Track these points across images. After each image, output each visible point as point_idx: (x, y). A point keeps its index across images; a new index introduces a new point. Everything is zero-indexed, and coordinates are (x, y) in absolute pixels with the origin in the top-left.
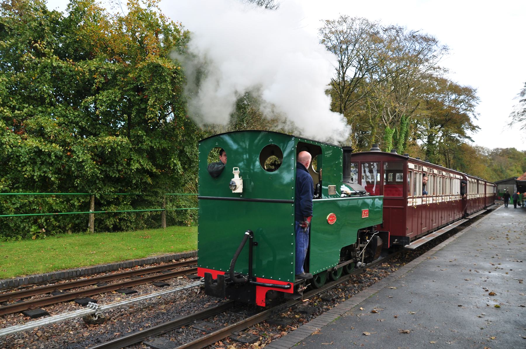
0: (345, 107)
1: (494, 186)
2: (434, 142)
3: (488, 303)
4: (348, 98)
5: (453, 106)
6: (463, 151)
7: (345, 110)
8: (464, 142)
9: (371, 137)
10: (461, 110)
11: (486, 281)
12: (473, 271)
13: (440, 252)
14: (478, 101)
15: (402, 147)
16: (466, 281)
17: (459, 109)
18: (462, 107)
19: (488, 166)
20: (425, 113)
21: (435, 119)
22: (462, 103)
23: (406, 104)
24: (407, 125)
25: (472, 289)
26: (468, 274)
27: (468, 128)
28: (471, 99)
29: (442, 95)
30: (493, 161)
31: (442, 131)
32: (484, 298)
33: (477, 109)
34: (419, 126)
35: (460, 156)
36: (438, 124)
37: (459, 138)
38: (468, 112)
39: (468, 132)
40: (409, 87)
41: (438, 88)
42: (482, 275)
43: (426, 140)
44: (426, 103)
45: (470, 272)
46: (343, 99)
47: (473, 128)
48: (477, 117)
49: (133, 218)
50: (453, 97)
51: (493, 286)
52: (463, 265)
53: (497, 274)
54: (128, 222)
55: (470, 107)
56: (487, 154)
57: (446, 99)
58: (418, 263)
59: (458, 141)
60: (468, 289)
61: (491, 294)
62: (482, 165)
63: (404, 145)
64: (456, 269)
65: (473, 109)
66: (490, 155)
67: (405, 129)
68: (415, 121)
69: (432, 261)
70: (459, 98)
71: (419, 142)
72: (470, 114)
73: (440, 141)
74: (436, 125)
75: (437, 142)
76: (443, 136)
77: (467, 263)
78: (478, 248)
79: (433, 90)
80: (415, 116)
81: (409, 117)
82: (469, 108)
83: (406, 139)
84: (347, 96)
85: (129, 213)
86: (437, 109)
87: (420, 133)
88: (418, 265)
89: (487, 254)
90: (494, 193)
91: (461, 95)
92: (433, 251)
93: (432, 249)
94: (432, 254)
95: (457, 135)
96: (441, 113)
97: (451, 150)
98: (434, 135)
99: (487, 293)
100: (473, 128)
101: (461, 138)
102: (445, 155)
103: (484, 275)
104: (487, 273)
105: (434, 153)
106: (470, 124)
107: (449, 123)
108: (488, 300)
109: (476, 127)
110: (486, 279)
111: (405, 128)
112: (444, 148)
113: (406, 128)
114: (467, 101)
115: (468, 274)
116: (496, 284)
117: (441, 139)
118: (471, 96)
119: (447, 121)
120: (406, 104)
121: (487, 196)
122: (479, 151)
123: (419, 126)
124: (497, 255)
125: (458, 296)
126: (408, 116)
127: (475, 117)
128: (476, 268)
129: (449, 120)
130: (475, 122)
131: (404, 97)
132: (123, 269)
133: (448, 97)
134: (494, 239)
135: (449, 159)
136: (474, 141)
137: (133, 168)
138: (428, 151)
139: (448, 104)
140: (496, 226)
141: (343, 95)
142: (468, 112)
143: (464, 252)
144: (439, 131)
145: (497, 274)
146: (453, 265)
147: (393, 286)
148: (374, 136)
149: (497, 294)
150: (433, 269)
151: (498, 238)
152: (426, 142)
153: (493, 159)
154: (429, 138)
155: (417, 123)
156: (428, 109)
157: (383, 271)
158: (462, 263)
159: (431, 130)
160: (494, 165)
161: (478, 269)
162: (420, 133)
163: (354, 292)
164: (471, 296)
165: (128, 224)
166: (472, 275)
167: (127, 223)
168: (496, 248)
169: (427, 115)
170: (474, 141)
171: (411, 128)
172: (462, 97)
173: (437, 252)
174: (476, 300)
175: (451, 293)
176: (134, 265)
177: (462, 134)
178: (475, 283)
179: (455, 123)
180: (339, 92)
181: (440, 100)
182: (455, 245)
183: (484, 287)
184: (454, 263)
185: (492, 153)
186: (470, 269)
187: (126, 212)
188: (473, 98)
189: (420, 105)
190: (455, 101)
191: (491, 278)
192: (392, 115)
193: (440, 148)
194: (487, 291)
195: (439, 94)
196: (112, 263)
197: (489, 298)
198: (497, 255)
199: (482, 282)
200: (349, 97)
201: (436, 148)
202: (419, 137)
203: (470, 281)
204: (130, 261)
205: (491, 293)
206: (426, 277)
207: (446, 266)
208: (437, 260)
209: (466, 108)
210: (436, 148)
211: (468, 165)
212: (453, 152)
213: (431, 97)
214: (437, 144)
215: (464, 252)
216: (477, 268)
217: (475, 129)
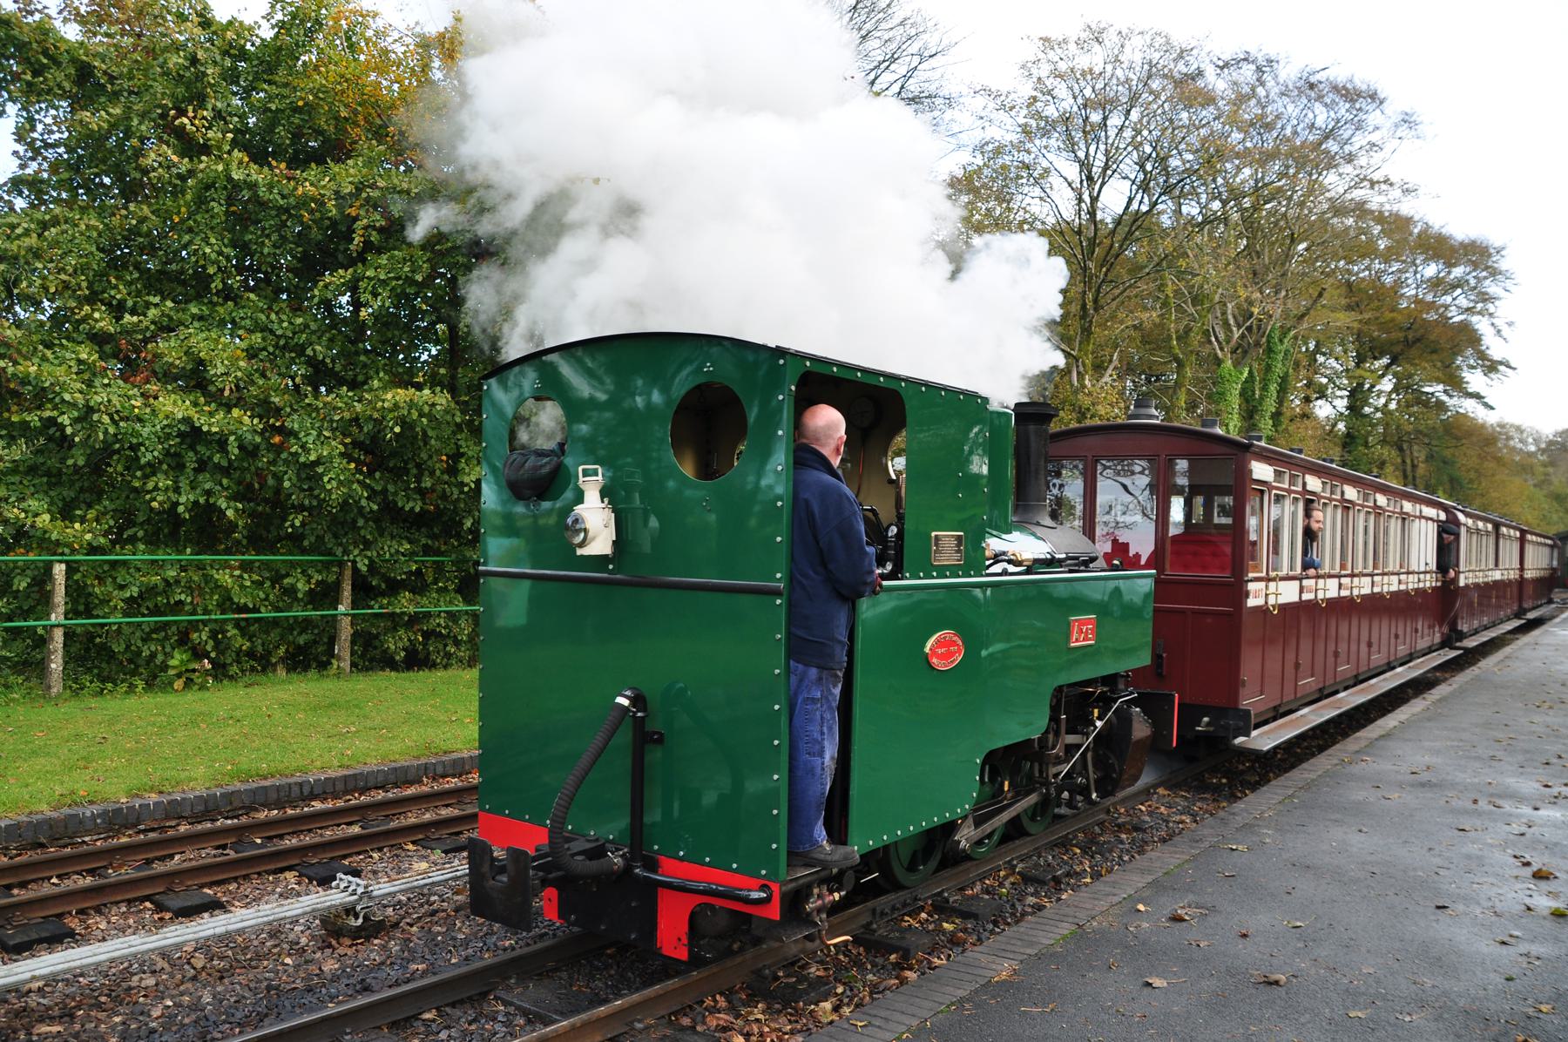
0: (1096, 301)
1: (1552, 547)
2: (1367, 410)
3: (1528, 901)
4: (1106, 275)
5: (1429, 298)
6: (1458, 439)
7: (1096, 310)
8: (1461, 411)
9: (1175, 392)
10: (1453, 312)
11: (1522, 835)
12: (1483, 804)
13: (1382, 743)
14: (1508, 284)
15: (1271, 422)
16: (1461, 833)
17: (1447, 307)
18: (1457, 302)
19: (1535, 486)
20: (1344, 319)
21: (1372, 340)
22: (1459, 291)
23: (1283, 293)
24: (1285, 358)
25: (1479, 858)
26: (1466, 812)
27: (1473, 367)
28: (1486, 278)
30: (1550, 470)
31: (1395, 375)
32: (1519, 886)
33: (1503, 309)
34: (1321, 359)
35: (1447, 453)
37: (1444, 398)
38: (1475, 319)
39: (1475, 380)
40: (1293, 240)
41: (1382, 244)
42: (1511, 815)
43: (1345, 402)
44: (1344, 290)
45: (1474, 806)
47: (1491, 367)
48: (1506, 331)
49: (464, 629)
50: (1431, 270)
51: (1547, 852)
52: (1453, 785)
53: (1558, 815)
54: (450, 642)
55: (1484, 301)
56: (1533, 448)
57: (1407, 279)
58: (1313, 776)
59: (1441, 406)
60: (1469, 857)
61: (1539, 876)
62: (1517, 481)
63: (1276, 416)
64: (1429, 795)
65: (1491, 308)
66: (1544, 451)
67: (1279, 369)
69: (1356, 769)
70: (1449, 273)
71: (1323, 410)
72: (1481, 324)
73: (1386, 405)
74: (1375, 358)
75: (1377, 409)
76: (1396, 390)
77: (1465, 777)
78: (1500, 736)
79: (1369, 251)
81: (1292, 333)
82: (1480, 306)
83: (1281, 401)
84: (1102, 266)
85: (452, 616)
86: (1377, 309)
87: (1324, 381)
88: (1313, 780)
89: (1527, 752)
90: (1553, 569)
91: (1455, 265)
92: (1360, 738)
93: (1358, 734)
94: (1356, 748)
95: (1441, 387)
96: (1393, 320)
98: (1367, 386)
99: (1528, 871)
100: (1491, 367)
101: (1451, 396)
102: (1401, 449)
103: (1519, 816)
104: (1526, 810)
105: (1367, 442)
106: (1482, 356)
107: (1414, 352)
108: (1529, 892)
109: (1501, 363)
110: (1524, 829)
111: (1279, 365)
112: (1398, 427)
113: (1284, 365)
114: (1473, 282)
115: (1466, 812)
116: (1556, 844)
117: (1389, 400)
118: (1487, 268)
119: (1409, 344)
120: (1283, 293)
121: (1528, 575)
122: (1509, 438)
123: (1321, 359)
124: (1560, 757)
125: (1436, 878)
126: (1289, 330)
127: (1499, 331)
128: (1492, 795)
130: (1495, 348)
132: (434, 779)
133: (1416, 272)
134: (1551, 708)
136: (1492, 408)
137: (466, 479)
138: (1348, 435)
139: (1414, 292)
140: (1558, 667)
141: (1091, 265)
142: (1475, 319)
143: (1456, 743)
144: (1383, 376)
145: (1558, 815)
146: (1423, 785)
148: (1183, 389)
149: (1558, 874)
150: (1359, 794)
151: (1562, 706)
153: (1552, 464)
154: (1353, 394)
155: (1317, 350)
156: (1349, 308)
158: (1450, 777)
159: (1359, 372)
160: (1555, 481)
161: (1500, 796)
162: (1324, 381)
164: (1476, 880)
165: (448, 648)
166: (1479, 814)
167: (446, 645)
168: (1557, 736)
170: (1492, 408)
171: (1297, 365)
172: (1458, 272)
173: (1372, 743)
174: (1493, 892)
175: (1415, 869)
176: (467, 767)
177: (1456, 384)
178: (1490, 841)
179: (1434, 352)
180: (1080, 257)
182: (1428, 724)
183: (1518, 854)
184: (1425, 776)
185: (1550, 443)
186: (1474, 796)
187: (445, 612)
188: (1494, 273)
189: (1326, 294)
190: (1436, 284)
191: (1541, 826)
192: (1239, 327)
193: (1387, 426)
194: (1528, 864)
195: (1387, 261)
196: (403, 762)
197: (1531, 886)
198: (1560, 757)
199: (1511, 837)
200: (1108, 270)
201: (1373, 426)
203: (1472, 834)
204: (455, 756)
205: (1540, 870)
206: (1337, 816)
207: (1401, 786)
208: (1372, 765)
209: (1471, 305)
210: (1373, 426)
211: (1471, 481)
212: (1427, 441)
215: (1456, 743)
216: (1498, 796)
217: (1497, 371)
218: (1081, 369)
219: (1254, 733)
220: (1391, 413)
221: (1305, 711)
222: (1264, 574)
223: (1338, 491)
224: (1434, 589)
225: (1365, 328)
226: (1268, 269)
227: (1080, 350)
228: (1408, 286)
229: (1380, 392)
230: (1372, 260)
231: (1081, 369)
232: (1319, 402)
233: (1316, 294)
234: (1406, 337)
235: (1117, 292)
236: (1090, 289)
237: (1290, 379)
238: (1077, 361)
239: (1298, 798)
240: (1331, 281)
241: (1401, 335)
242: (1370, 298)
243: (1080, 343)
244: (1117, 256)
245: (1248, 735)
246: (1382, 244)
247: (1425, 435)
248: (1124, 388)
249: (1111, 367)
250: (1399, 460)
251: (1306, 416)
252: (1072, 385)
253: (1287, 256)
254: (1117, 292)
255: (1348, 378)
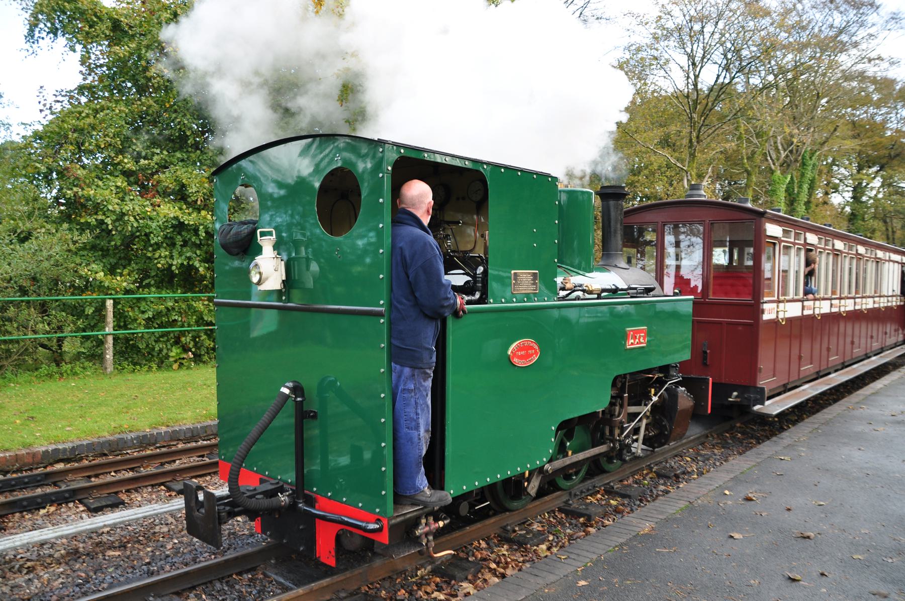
0: (698, 137)
2: (864, 199)
4: (704, 121)
7: (698, 142)
9: (746, 191)
13: (873, 397)
15: (804, 207)
20: (850, 144)
21: (868, 156)
23: (812, 129)
29: (884, 110)
31: (882, 177)
34: (835, 168)
36: (874, 165)
40: (818, 97)
41: (875, 97)
43: (850, 194)
44: (850, 126)
46: (695, 124)
57: (891, 118)
58: (830, 417)
67: (809, 175)
68: (830, 161)
69: (857, 413)
71: (836, 199)
73: (876, 195)
74: (870, 167)
75: (870, 198)
76: (882, 186)
79: (867, 101)
80: (830, 151)
81: (818, 153)
84: (702, 116)
93: (858, 392)
94: (857, 400)
97: (898, 211)
98: (864, 184)
102: (885, 222)
107: (895, 162)
117: (879, 192)
119: (891, 158)
120: (812, 129)
123: (835, 168)
126: (816, 151)
129: (898, 155)
131: (809, 116)
135: (892, 229)
138: (852, 214)
141: (695, 116)
144: (874, 178)
146: (899, 423)
147: (785, 456)
148: (751, 189)
150: (859, 428)
152: (849, 199)
154: (855, 190)
155: (833, 163)
156: (854, 137)
157: (767, 428)
162: (837, 181)
163: (714, 463)
169: (853, 149)
171: (820, 172)
173: (867, 398)
180: (688, 111)
181: (878, 119)
189: (839, 129)
193: (876, 208)
200: (705, 119)
201: (868, 208)
202: (836, 189)
206: (846, 440)
208: (867, 411)
210: (868, 208)
213: (861, 114)
214: (872, 201)
218: (689, 178)
219: (767, 403)
220: (879, 200)
221: (806, 386)
222: (775, 298)
223: (802, 237)
224: (898, 306)
225: (864, 149)
226: (803, 115)
227: (688, 167)
228: (891, 122)
229: (872, 189)
230: (869, 107)
231: (689, 178)
232: (834, 195)
233: (833, 129)
234: (890, 154)
235: (710, 131)
236: (694, 130)
237: (816, 181)
238: (687, 173)
239: (821, 429)
240: (842, 121)
241: (886, 152)
242: (867, 130)
243: (689, 162)
244: (711, 110)
245: (763, 404)
246: (875, 97)
247: (901, 213)
248: (715, 188)
249: (707, 176)
250: (884, 228)
251: (825, 203)
252: (684, 188)
253: (815, 107)
254: (710, 131)
255: (853, 180)
